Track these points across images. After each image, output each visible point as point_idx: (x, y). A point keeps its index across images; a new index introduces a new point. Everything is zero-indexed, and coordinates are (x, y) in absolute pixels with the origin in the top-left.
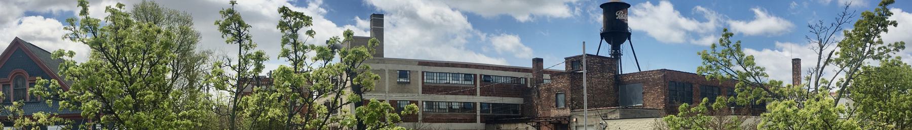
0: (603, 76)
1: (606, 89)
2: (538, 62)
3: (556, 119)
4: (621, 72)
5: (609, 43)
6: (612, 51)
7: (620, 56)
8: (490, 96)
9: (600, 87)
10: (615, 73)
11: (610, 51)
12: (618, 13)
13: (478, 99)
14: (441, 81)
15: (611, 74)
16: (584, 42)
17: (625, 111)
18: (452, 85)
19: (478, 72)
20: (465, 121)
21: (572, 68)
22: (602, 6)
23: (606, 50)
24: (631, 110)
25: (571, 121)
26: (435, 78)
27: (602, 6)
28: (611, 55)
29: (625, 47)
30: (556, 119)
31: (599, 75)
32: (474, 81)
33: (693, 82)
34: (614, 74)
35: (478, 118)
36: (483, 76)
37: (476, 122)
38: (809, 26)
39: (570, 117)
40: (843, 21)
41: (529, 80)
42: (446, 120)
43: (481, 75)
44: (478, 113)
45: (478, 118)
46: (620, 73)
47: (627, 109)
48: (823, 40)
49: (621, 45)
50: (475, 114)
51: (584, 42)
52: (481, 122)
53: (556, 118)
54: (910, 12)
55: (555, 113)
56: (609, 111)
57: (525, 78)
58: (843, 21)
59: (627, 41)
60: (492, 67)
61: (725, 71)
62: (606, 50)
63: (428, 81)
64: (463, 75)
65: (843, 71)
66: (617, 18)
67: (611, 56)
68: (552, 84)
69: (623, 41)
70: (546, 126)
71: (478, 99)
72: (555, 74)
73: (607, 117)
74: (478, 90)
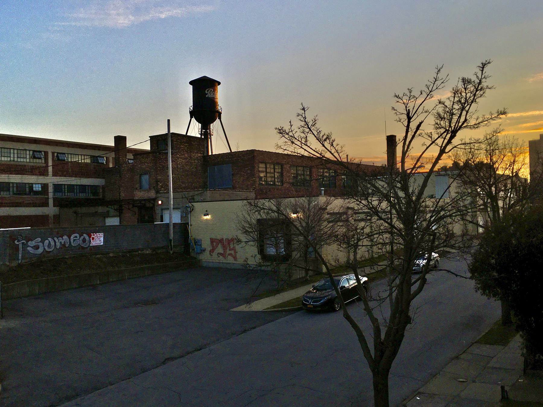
0: (190, 157)
1: (194, 170)
2: (120, 140)
4: (212, 152)
5: (199, 122)
6: (201, 131)
7: (210, 136)
8: (65, 176)
9: (187, 168)
10: (203, 154)
11: (200, 130)
12: (208, 91)
13: (51, 180)
14: (19, 160)
15: (199, 155)
16: (169, 121)
17: (212, 193)
18: (17, 163)
19: (50, 149)
20: (34, 205)
21: (158, 147)
22: (191, 83)
23: (195, 130)
24: (219, 192)
25: (156, 204)
26: (12, 156)
27: (191, 83)
28: (201, 134)
29: (215, 126)
31: (186, 155)
32: (45, 159)
33: (284, 163)
34: (202, 155)
35: (51, 202)
36: (56, 154)
37: (48, 206)
38: (396, 96)
39: (155, 200)
40: (435, 88)
42: (9, 203)
44: (51, 195)
45: (51, 202)
46: (210, 154)
47: (215, 192)
48: (411, 110)
49: (212, 125)
50: (47, 197)
51: (169, 121)
52: (54, 206)
53: (140, 201)
55: (139, 195)
56: (196, 193)
58: (435, 88)
59: (218, 120)
61: (301, 147)
62: (195, 130)
63: (19, 160)
64: (31, 153)
65: (434, 144)
66: (207, 96)
67: (201, 136)
68: (135, 164)
69: (213, 121)
70: (129, 209)
72: (138, 153)
73: (194, 199)
74: (50, 169)
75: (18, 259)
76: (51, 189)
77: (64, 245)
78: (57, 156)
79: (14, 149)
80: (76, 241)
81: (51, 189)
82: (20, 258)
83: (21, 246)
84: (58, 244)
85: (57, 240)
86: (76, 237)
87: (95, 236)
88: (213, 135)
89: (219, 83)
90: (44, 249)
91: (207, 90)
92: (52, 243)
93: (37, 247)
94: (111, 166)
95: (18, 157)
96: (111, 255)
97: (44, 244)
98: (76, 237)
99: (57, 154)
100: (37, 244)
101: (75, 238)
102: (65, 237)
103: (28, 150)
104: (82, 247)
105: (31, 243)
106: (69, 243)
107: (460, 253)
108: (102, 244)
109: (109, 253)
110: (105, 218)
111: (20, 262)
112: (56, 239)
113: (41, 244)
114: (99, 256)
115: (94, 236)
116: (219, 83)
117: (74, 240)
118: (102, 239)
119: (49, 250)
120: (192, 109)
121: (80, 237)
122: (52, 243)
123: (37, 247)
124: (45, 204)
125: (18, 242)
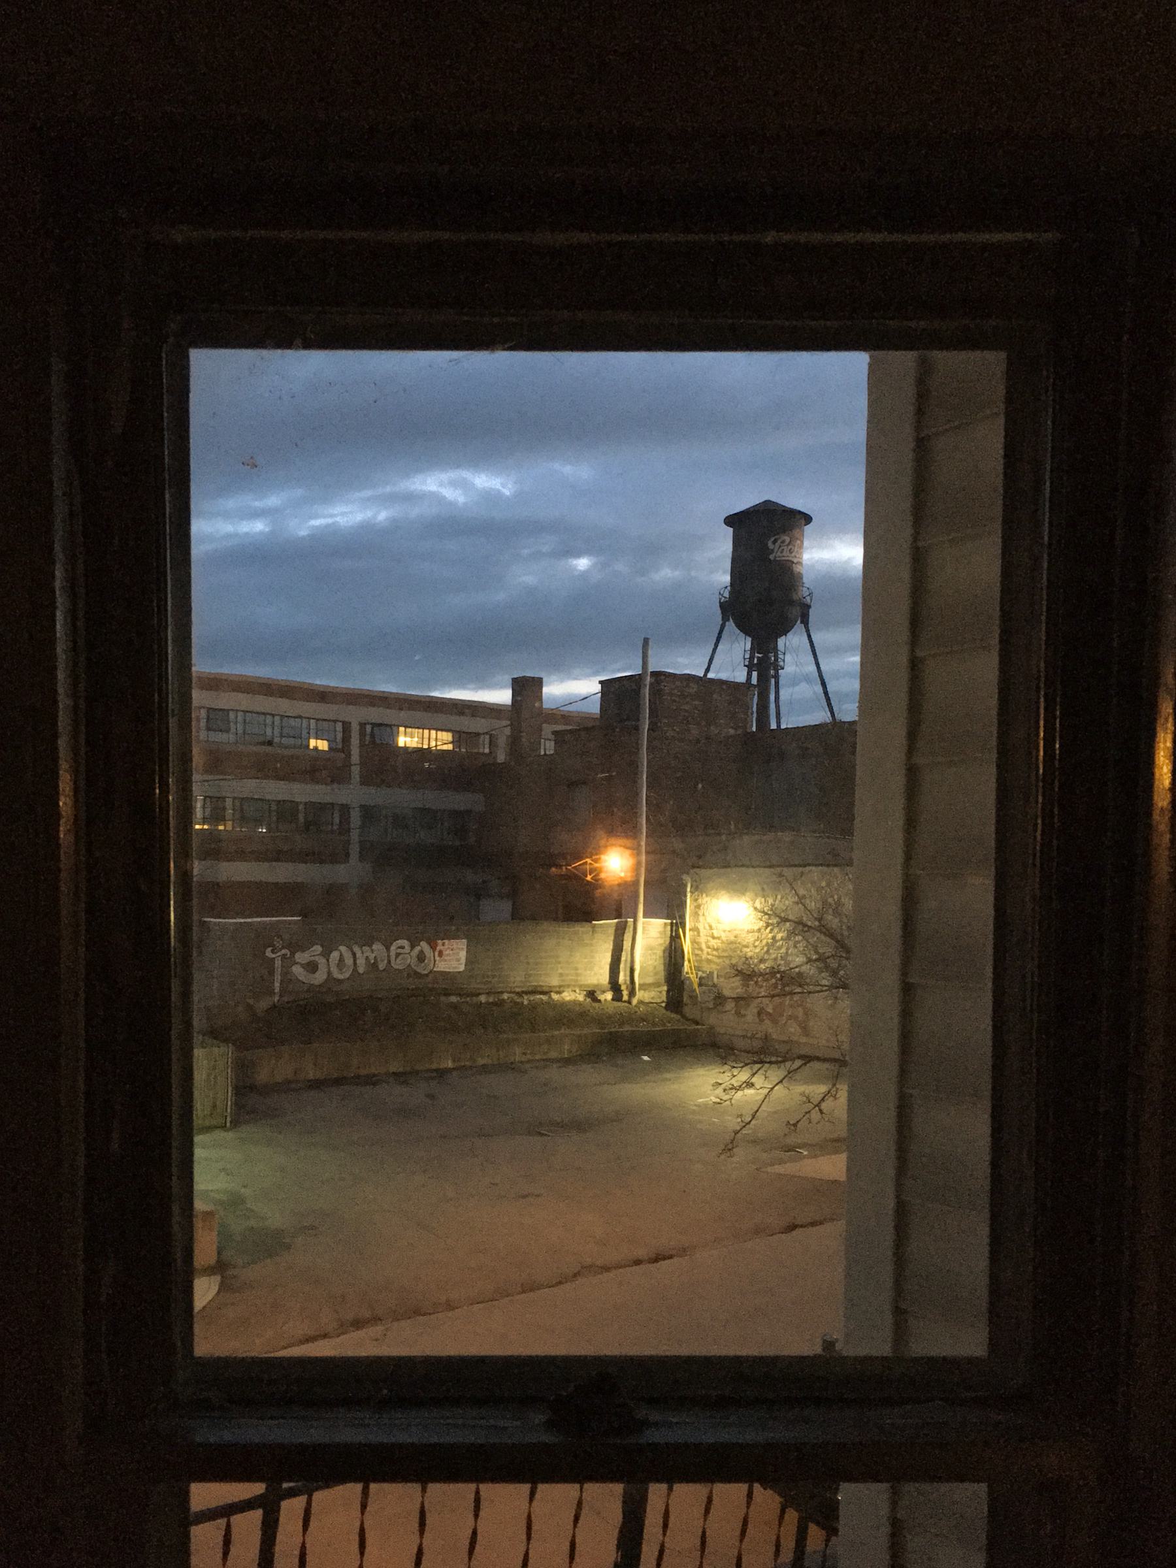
3: (844, 838)
6: (752, 658)
11: (747, 656)
12: (774, 542)
22: (730, 521)
27: (730, 521)
29: (792, 645)
30: (844, 838)
35: (354, 849)
36: (369, 728)
41: (355, 728)
43: (362, 725)
45: (354, 849)
46: (774, 726)
54: (259, 1565)
57: (344, 723)
59: (799, 626)
60: (367, 696)
66: (772, 557)
71: (353, 794)
74: (356, 771)
75: (272, 993)
76: (355, 818)
77: (374, 966)
78: (372, 735)
79: (273, 715)
80: (400, 957)
81: (355, 818)
82: (276, 991)
83: (278, 963)
84: (361, 961)
85: (359, 954)
86: (403, 947)
87: (446, 947)
88: (783, 669)
89: (808, 519)
90: (329, 973)
91: (773, 539)
92: (349, 961)
93: (312, 967)
94: (501, 757)
95: (282, 736)
96: (483, 999)
97: (328, 960)
98: (403, 947)
99: (372, 728)
100: (313, 958)
101: (399, 951)
102: (377, 946)
103: (305, 718)
104: (416, 973)
105: (302, 957)
106: (386, 962)
107: (307, 927)
108: (462, 968)
109: (480, 994)
110: (478, 897)
111: (276, 999)
112: (356, 949)
113: (322, 961)
114: (454, 999)
115: (442, 948)
116: (808, 519)
117: (398, 955)
118: (463, 955)
119: (341, 977)
120: (727, 594)
121: (412, 947)
122: (349, 961)
123: (312, 967)
124: (338, 856)
125: (273, 952)
